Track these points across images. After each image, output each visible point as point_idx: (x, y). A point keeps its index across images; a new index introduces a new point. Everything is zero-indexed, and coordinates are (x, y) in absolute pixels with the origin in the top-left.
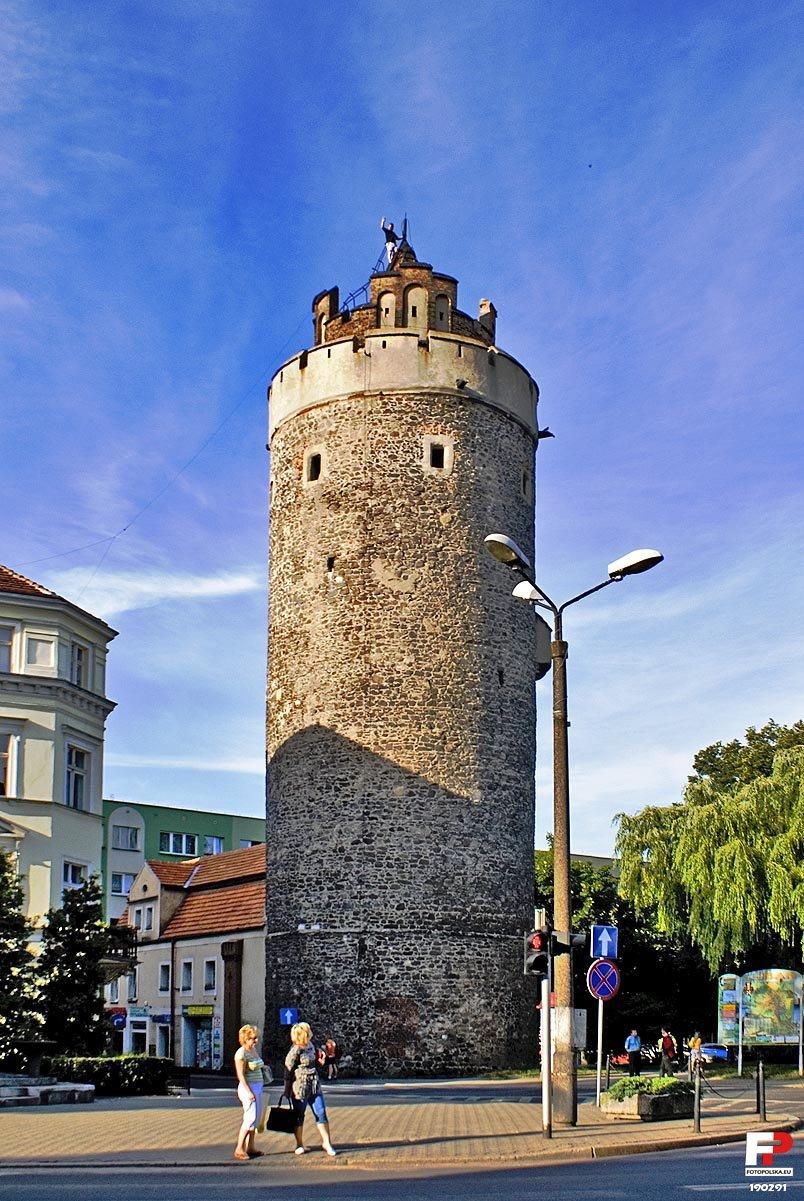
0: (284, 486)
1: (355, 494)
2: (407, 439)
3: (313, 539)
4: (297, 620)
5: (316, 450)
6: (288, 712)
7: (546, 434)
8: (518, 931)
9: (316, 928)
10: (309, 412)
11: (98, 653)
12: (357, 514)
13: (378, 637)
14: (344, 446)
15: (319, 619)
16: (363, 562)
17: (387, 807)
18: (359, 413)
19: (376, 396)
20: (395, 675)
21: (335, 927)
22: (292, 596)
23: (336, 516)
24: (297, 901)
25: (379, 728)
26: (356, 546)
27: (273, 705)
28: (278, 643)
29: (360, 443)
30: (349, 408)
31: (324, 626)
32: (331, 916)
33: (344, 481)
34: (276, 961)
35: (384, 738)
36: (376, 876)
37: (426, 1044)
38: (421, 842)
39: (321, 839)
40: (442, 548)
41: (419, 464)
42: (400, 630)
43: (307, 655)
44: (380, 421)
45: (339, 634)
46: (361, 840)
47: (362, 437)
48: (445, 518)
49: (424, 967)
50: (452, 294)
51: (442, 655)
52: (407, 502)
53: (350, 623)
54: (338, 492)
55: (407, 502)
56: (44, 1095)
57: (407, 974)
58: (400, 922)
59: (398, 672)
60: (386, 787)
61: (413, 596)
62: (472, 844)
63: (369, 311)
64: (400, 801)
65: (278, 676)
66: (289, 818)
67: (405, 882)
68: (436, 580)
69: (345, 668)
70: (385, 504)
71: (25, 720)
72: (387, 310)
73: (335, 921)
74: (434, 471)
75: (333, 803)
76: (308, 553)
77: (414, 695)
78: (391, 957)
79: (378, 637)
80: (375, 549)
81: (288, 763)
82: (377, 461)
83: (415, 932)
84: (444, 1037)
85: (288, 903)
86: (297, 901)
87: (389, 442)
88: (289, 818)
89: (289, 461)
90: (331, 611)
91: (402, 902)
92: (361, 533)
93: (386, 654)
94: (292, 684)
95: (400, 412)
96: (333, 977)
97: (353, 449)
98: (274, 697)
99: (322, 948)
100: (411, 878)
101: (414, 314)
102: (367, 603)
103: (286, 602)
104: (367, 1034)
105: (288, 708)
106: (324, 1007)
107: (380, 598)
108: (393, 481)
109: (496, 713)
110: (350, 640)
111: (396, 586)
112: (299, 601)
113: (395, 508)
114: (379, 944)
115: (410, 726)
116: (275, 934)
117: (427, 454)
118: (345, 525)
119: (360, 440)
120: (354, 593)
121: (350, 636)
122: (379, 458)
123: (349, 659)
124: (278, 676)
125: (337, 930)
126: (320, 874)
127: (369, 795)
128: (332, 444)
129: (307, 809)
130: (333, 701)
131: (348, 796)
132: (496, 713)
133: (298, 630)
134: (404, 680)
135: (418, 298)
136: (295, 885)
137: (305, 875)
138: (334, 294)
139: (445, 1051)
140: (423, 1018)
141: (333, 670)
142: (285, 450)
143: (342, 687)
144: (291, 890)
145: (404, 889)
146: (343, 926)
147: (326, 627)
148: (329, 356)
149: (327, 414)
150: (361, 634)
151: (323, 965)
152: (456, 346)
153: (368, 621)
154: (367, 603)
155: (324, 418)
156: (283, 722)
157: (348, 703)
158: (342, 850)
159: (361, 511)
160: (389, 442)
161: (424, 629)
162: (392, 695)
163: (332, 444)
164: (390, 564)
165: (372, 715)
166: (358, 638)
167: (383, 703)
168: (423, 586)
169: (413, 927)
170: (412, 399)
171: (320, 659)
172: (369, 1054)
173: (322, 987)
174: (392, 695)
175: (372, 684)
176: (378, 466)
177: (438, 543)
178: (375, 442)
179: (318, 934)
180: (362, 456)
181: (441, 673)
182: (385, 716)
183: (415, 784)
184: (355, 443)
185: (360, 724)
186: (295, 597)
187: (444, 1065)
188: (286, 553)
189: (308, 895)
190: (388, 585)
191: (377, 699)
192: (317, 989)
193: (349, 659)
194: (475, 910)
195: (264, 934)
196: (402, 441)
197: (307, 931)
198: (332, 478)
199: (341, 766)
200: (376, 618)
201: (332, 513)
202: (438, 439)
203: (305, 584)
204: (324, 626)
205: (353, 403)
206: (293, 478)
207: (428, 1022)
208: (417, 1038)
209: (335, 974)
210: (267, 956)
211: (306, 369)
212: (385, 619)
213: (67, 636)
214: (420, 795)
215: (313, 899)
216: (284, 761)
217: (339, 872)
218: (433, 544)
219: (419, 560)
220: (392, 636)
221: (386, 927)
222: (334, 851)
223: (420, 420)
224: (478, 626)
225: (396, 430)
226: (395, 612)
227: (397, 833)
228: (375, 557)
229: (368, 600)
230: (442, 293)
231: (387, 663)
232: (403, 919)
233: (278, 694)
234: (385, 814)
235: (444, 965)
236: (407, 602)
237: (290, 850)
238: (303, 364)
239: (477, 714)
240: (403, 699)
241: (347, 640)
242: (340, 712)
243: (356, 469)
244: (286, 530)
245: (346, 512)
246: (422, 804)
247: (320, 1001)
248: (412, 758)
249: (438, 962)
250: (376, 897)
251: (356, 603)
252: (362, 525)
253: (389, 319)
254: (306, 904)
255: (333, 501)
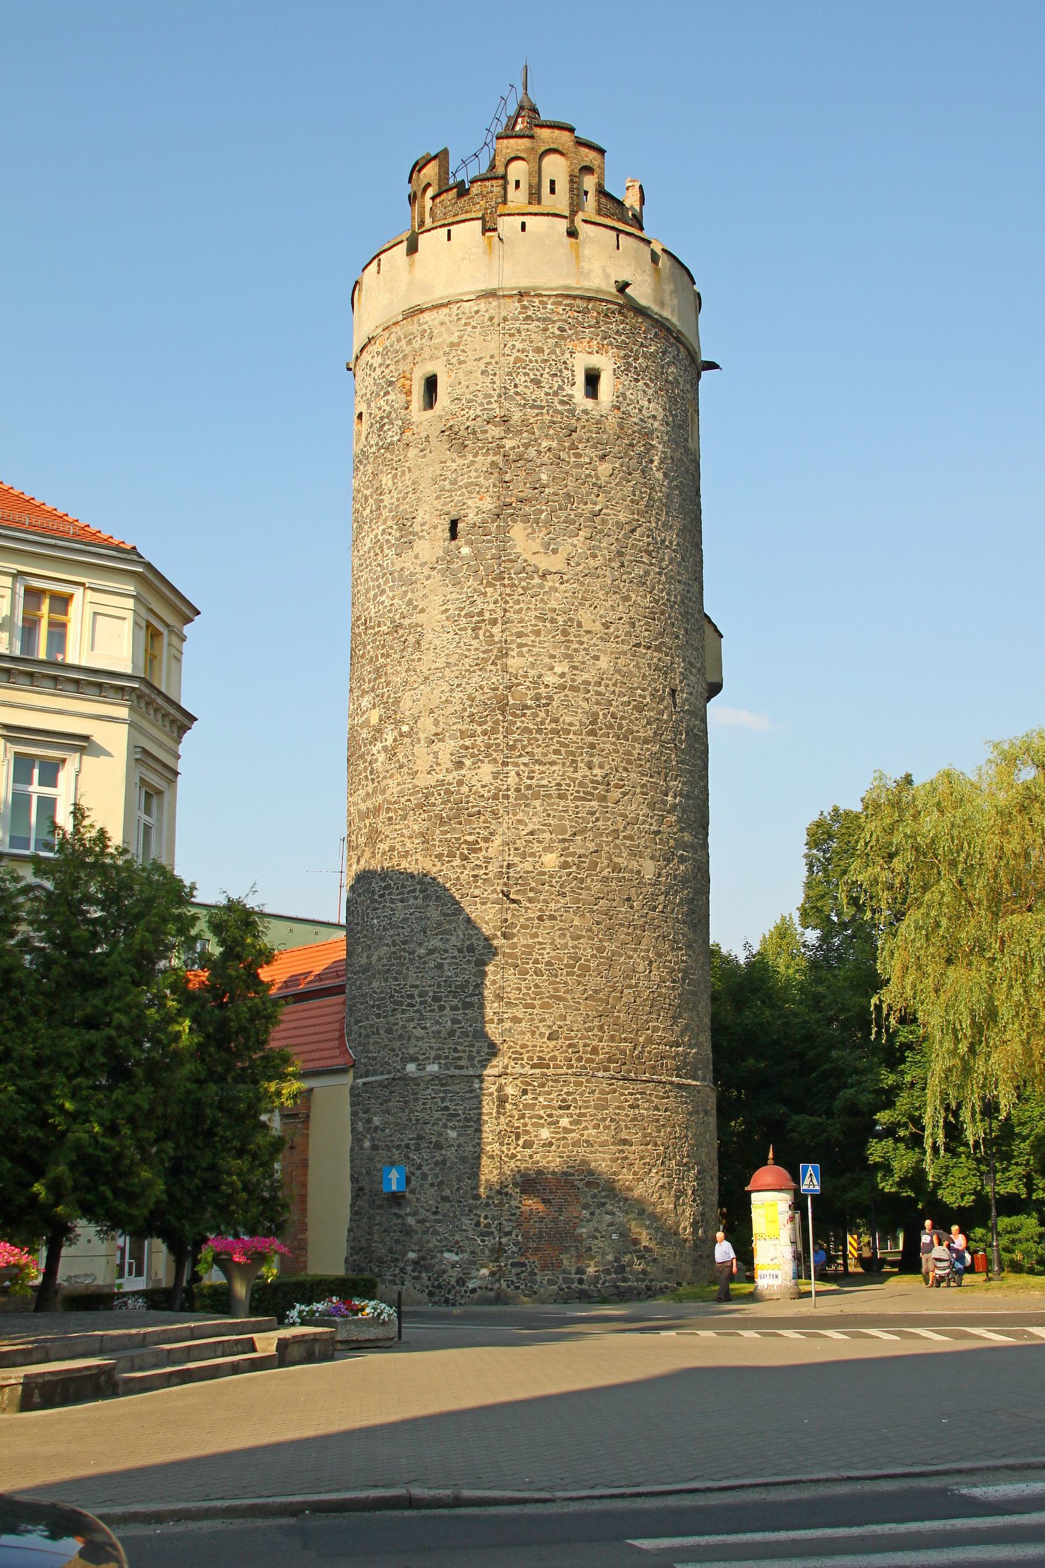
0: (382, 418)
1: (486, 432)
2: (554, 357)
3: (428, 493)
4: (404, 609)
5: (429, 368)
6: (389, 742)
7: (712, 366)
8: (700, 1072)
9: (433, 1068)
10: (421, 316)
11: (175, 640)
12: (490, 458)
13: (520, 635)
14: (470, 365)
15: (436, 605)
16: (498, 526)
17: (533, 884)
18: (491, 319)
19: (511, 296)
20: (543, 690)
21: (461, 1068)
22: (396, 575)
23: (461, 461)
24: (404, 1027)
25: (522, 767)
26: (488, 504)
27: (364, 733)
28: (374, 641)
29: (493, 361)
30: (477, 312)
31: (444, 617)
32: (456, 1050)
33: (471, 412)
34: (369, 1121)
35: (529, 782)
36: (520, 989)
37: (590, 1249)
38: (579, 937)
39: (440, 933)
40: (600, 510)
41: (570, 392)
42: (548, 625)
43: (420, 660)
44: (519, 332)
45: (465, 629)
46: (499, 934)
47: (495, 353)
48: (604, 468)
49: (586, 1128)
50: (599, 167)
51: (604, 663)
52: (554, 444)
53: (481, 613)
54: (462, 428)
55: (554, 444)
56: (283, 1345)
57: (564, 1138)
58: (554, 1058)
59: (547, 686)
60: (533, 855)
61: (565, 578)
62: (644, 941)
63: (494, 182)
64: (551, 876)
65: (373, 690)
66: (392, 901)
67: (560, 999)
68: (594, 556)
69: (475, 679)
70: (527, 446)
71: (86, 738)
72: (517, 183)
73: (460, 1058)
74: (589, 404)
75: (458, 878)
76: (421, 513)
77: (568, 719)
78: (542, 1113)
79: (520, 635)
80: (515, 508)
81: (390, 819)
82: (516, 386)
83: (574, 1074)
84: (614, 1236)
85: (389, 1031)
86: (404, 1027)
87: (531, 361)
88: (392, 901)
89: (391, 383)
90: (454, 596)
91: (555, 1028)
92: (495, 486)
93: (531, 659)
94: (397, 701)
95: (545, 320)
96: (459, 1146)
97: (483, 368)
98: (368, 720)
99: (443, 1099)
100: (567, 992)
101: (553, 191)
102: (504, 586)
103: (386, 582)
104: (509, 1233)
105: (389, 737)
106: (447, 1192)
107: (521, 579)
108: (537, 415)
109: (670, 749)
110: (482, 638)
111: (544, 563)
112: (408, 581)
113: (539, 452)
114: (525, 1092)
115: (564, 764)
116: (370, 1079)
117: (580, 379)
118: (473, 474)
119: (492, 357)
120: (485, 570)
121: (481, 632)
122: (517, 382)
123: (480, 665)
124: (373, 690)
125: (464, 1072)
126: (439, 986)
127: (509, 866)
128: (454, 361)
129: (418, 887)
130: (459, 726)
131: (479, 867)
132: (670, 749)
133: (406, 622)
134: (556, 697)
135: (556, 168)
136: (401, 1004)
137: (417, 987)
138: (443, 157)
139: (617, 1259)
140: (586, 1206)
141: (457, 682)
142: (383, 368)
143: (471, 706)
144: (394, 1010)
145: (559, 1009)
146: (473, 1066)
147: (447, 619)
148: (449, 239)
149: (447, 319)
150: (496, 630)
151: (445, 1126)
152: (614, 234)
153: (505, 611)
154: (504, 586)
155: (442, 324)
156: (382, 757)
157: (479, 729)
158: (471, 949)
159: (495, 455)
160: (531, 361)
161: (580, 625)
162: (539, 719)
163: (454, 361)
164: (534, 532)
165: (512, 748)
166: (492, 636)
167: (527, 730)
168: (578, 564)
169: (570, 1067)
170: (560, 304)
171: (438, 665)
172: (513, 1265)
173: (444, 1161)
174: (539, 719)
175: (511, 702)
176: (517, 393)
177: (595, 504)
178: (512, 359)
179: (435, 1078)
180: (496, 379)
181: (602, 689)
182: (529, 749)
183: (571, 850)
184: (485, 360)
185: (495, 760)
186: (401, 576)
187: (614, 1281)
188: (385, 513)
189: (422, 1018)
190: (533, 560)
191: (519, 724)
192: (436, 1163)
193: (480, 665)
194: (649, 1041)
195: (348, 1079)
196: (547, 361)
197: (420, 1074)
198: (454, 408)
199: (470, 822)
200: (517, 607)
201: (455, 456)
202: (597, 361)
203: (416, 557)
204: (444, 617)
205: (483, 305)
206: (396, 406)
207: (592, 1214)
208: (579, 1239)
209: (462, 1140)
210: (354, 1114)
211: (417, 255)
212: (528, 609)
213: (143, 612)
214: (578, 868)
215: (428, 1025)
216: (383, 816)
217: (467, 982)
218: (590, 506)
219: (571, 526)
220: (537, 633)
221: (533, 1067)
222: (460, 951)
223: (570, 332)
224: (647, 623)
225: (540, 344)
226: (542, 600)
227: (547, 923)
228: (515, 521)
229: (506, 582)
230: (588, 164)
231: (532, 672)
232: (557, 1053)
233: (374, 717)
234: (531, 895)
235: (613, 1126)
236: (557, 585)
237: (393, 949)
238: (413, 249)
239: (648, 749)
240: (554, 725)
241: (476, 637)
242: (468, 742)
243: (488, 396)
244: (386, 480)
245: (475, 456)
246: (582, 881)
247: (441, 1183)
248: (566, 811)
249: (604, 1120)
250: (520, 1021)
251: (490, 584)
252: (496, 475)
253: (517, 198)
254: (419, 1033)
255: (456, 438)
